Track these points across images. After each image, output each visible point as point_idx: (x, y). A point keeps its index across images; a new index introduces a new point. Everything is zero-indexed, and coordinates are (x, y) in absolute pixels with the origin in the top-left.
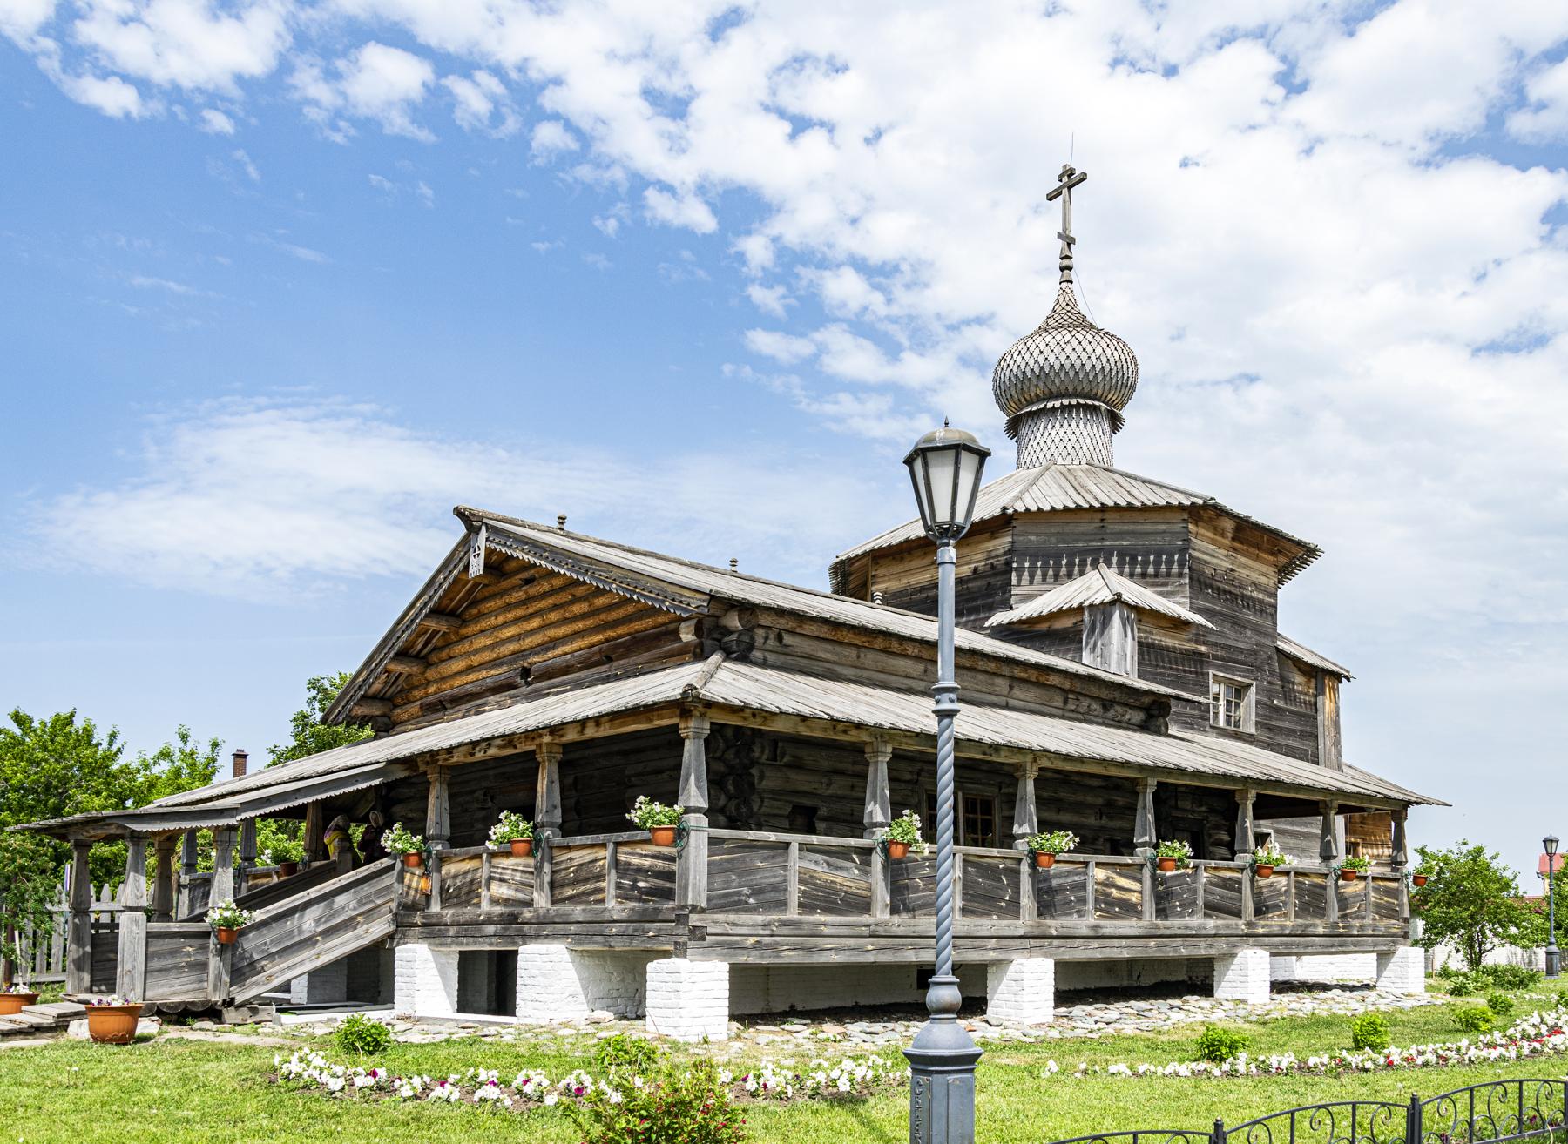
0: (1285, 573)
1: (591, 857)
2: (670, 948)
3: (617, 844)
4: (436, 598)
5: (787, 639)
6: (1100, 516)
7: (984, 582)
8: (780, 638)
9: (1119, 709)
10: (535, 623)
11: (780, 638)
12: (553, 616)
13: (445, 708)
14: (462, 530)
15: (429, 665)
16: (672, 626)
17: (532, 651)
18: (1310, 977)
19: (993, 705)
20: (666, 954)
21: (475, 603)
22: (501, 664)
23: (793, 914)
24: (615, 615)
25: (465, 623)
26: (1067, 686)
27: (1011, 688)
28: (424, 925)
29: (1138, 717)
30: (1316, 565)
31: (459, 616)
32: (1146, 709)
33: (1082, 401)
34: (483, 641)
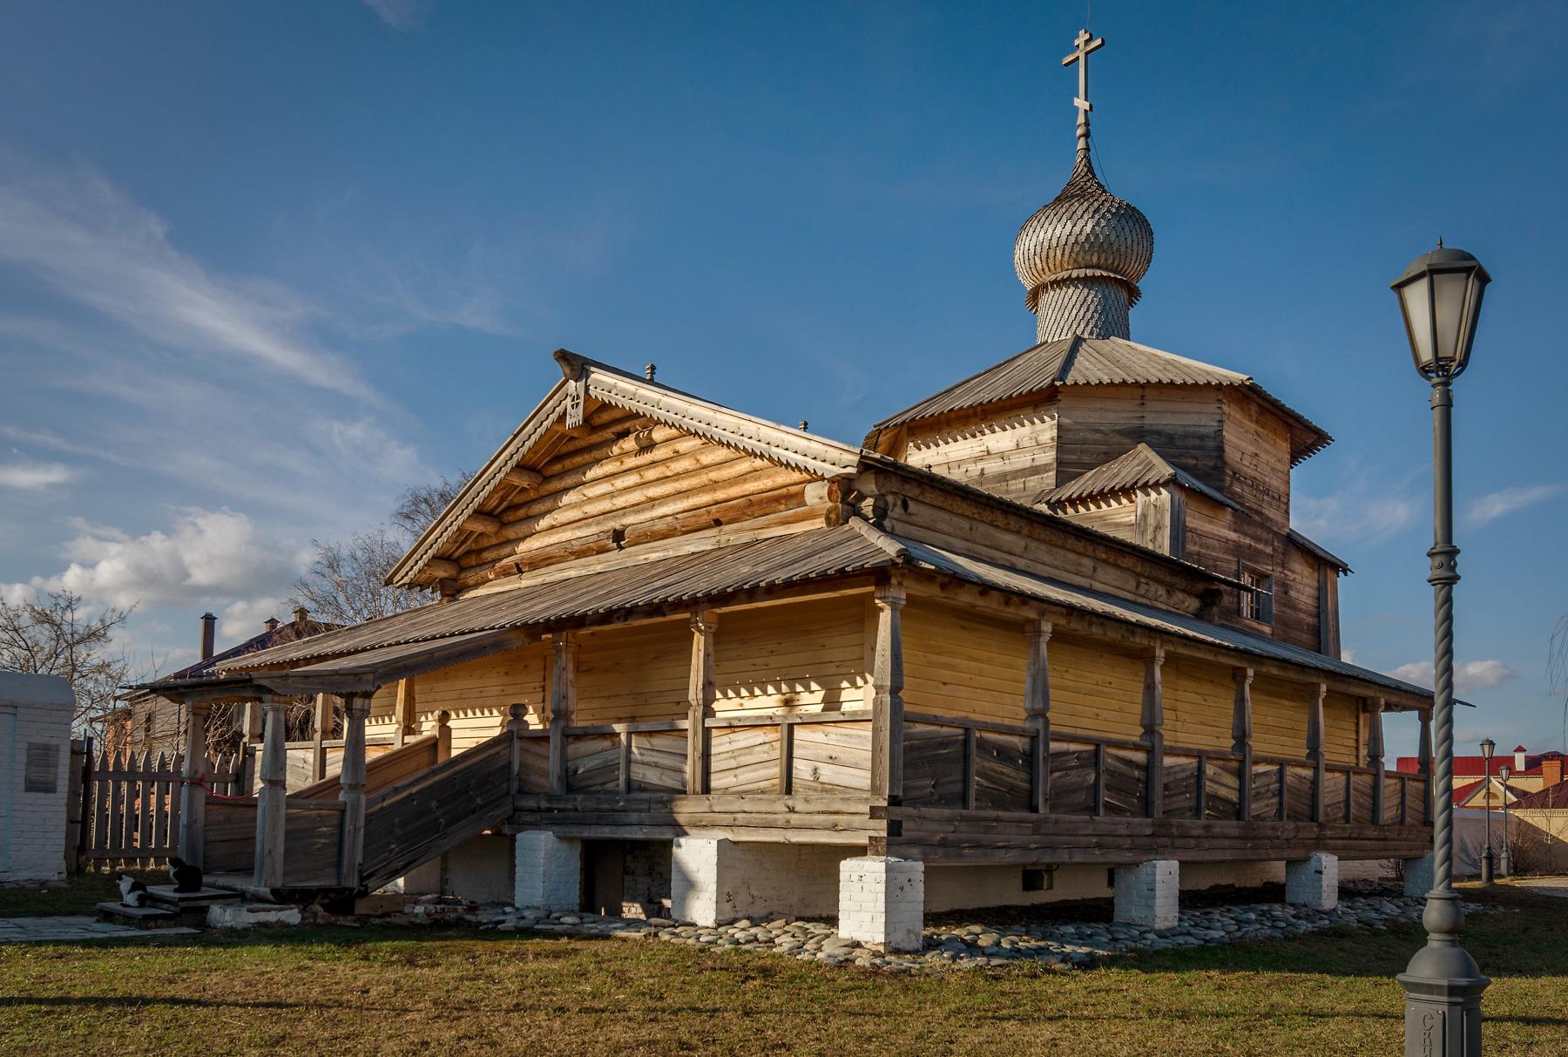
0: (1296, 456)
2: (865, 841)
4: (524, 449)
5: (912, 506)
6: (1140, 391)
8: (905, 506)
9: (1180, 595)
11: (905, 506)
12: (651, 474)
13: (520, 571)
16: (793, 489)
18: (337, 648)
19: (609, 616)
20: (858, 851)
21: (559, 458)
23: (972, 810)
25: (547, 479)
26: (1138, 570)
27: (1095, 569)
29: (1193, 604)
31: (539, 472)
32: (1200, 596)
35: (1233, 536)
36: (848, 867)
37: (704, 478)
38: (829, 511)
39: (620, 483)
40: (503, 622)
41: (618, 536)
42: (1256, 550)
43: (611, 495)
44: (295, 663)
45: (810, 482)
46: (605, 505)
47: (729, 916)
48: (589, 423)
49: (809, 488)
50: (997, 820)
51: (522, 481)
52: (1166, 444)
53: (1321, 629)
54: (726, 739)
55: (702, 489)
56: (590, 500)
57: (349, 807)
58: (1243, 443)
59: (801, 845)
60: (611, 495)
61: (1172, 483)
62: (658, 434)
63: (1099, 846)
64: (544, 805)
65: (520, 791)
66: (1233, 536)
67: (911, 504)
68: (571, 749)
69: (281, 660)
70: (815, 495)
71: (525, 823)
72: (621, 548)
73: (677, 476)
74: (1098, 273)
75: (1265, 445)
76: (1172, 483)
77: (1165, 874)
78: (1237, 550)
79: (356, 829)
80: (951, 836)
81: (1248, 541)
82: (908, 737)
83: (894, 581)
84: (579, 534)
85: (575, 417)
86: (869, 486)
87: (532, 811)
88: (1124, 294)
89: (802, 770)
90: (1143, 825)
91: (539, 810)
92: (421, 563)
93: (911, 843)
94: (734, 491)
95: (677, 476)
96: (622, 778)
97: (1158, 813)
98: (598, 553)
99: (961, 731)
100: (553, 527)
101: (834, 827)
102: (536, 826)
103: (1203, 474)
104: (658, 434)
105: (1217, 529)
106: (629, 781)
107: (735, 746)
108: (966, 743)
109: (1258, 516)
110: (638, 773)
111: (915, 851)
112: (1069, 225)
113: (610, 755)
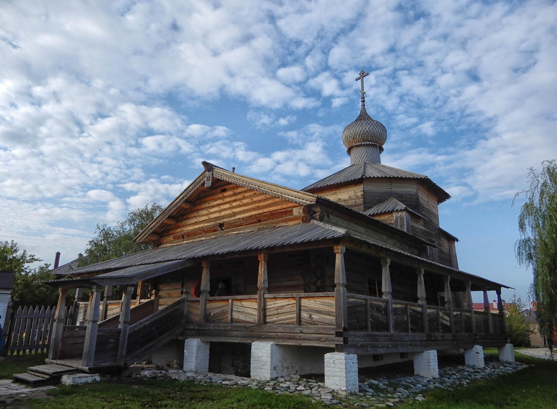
1: (288, 303)
2: (334, 346)
3: (300, 298)
4: (188, 195)
7: (354, 201)
8: (328, 216)
10: (227, 206)
11: (328, 216)
12: (234, 204)
14: (202, 168)
15: (178, 221)
17: (224, 217)
18: (117, 266)
20: (331, 350)
22: (210, 222)
23: (370, 332)
24: (262, 204)
28: (198, 330)
30: (447, 201)
33: (368, 143)
34: (205, 212)
35: (424, 228)
36: (327, 356)
37: (254, 206)
38: (303, 217)
39: (222, 207)
40: (184, 257)
41: (221, 225)
42: (431, 233)
43: (219, 211)
44: (98, 272)
45: (294, 207)
46: (217, 215)
47: (274, 376)
48: (212, 188)
49: (294, 209)
50: (379, 336)
51: (187, 206)
52: (401, 198)
53: (450, 258)
54: (272, 303)
55: (254, 209)
56: (211, 213)
57: (122, 331)
58: (424, 197)
59: (305, 347)
60: (219, 211)
61: (405, 210)
62: (110, 186)
63: (411, 345)
64: (196, 328)
65: (187, 322)
66: (424, 228)
67: (330, 215)
68: (208, 306)
69: (94, 270)
70: (297, 212)
71: (188, 335)
72: (222, 230)
73: (245, 205)
74: (371, 143)
75: (430, 199)
76: (405, 210)
77: (432, 355)
78: (424, 233)
79: (124, 340)
80: (364, 343)
81: (428, 230)
82: (348, 303)
83: (341, 243)
84: (206, 225)
85: (208, 184)
86: (318, 209)
87: (191, 330)
88: (378, 150)
89: (305, 315)
90: (419, 336)
91: (194, 329)
92: (147, 235)
93: (352, 346)
94: (266, 210)
95: (245, 205)
96: (230, 317)
97: (427, 331)
98: (214, 232)
99: (364, 301)
100: (196, 222)
101: (319, 340)
102: (193, 336)
103: (415, 209)
104: (110, 186)
105: (420, 226)
106: (232, 318)
107: (276, 305)
108: (366, 305)
109: (431, 221)
110: (236, 316)
111: (352, 350)
112: (361, 128)
113: (224, 308)
